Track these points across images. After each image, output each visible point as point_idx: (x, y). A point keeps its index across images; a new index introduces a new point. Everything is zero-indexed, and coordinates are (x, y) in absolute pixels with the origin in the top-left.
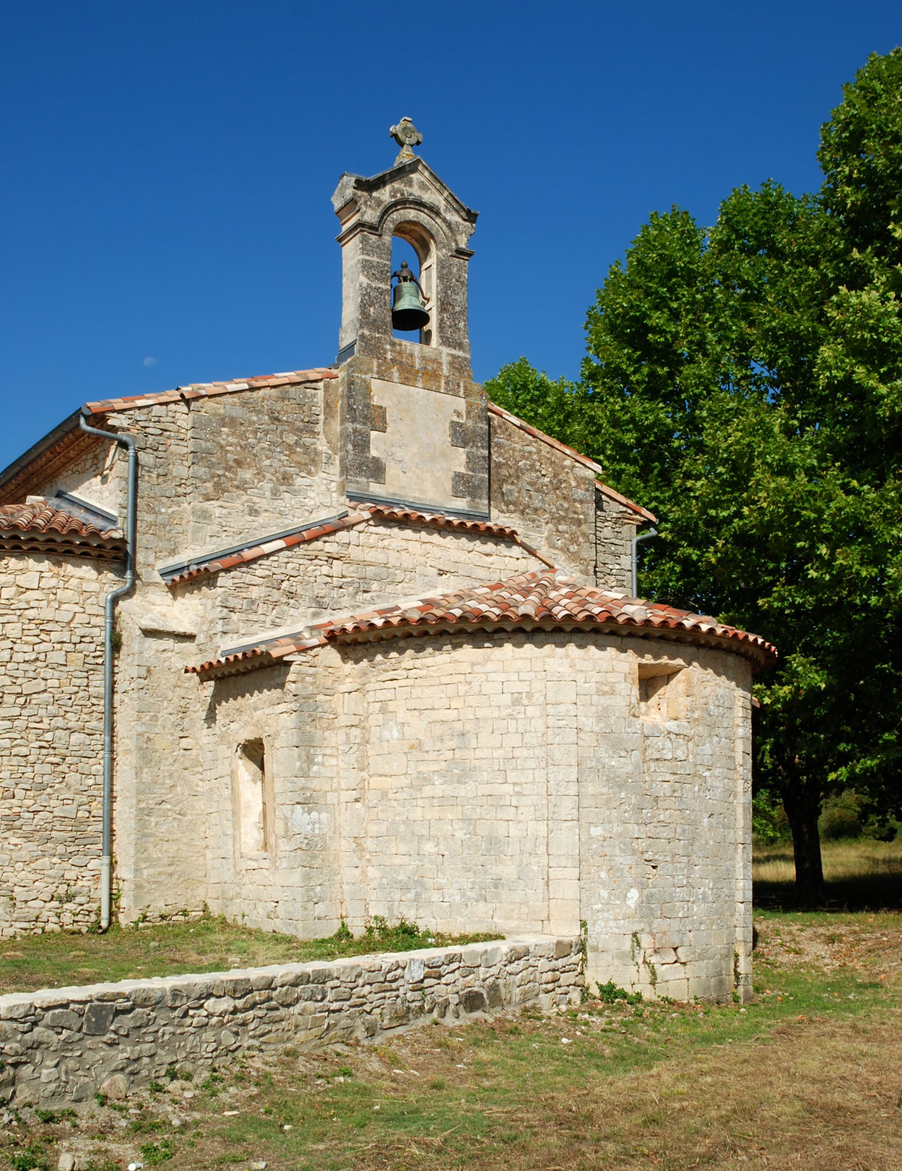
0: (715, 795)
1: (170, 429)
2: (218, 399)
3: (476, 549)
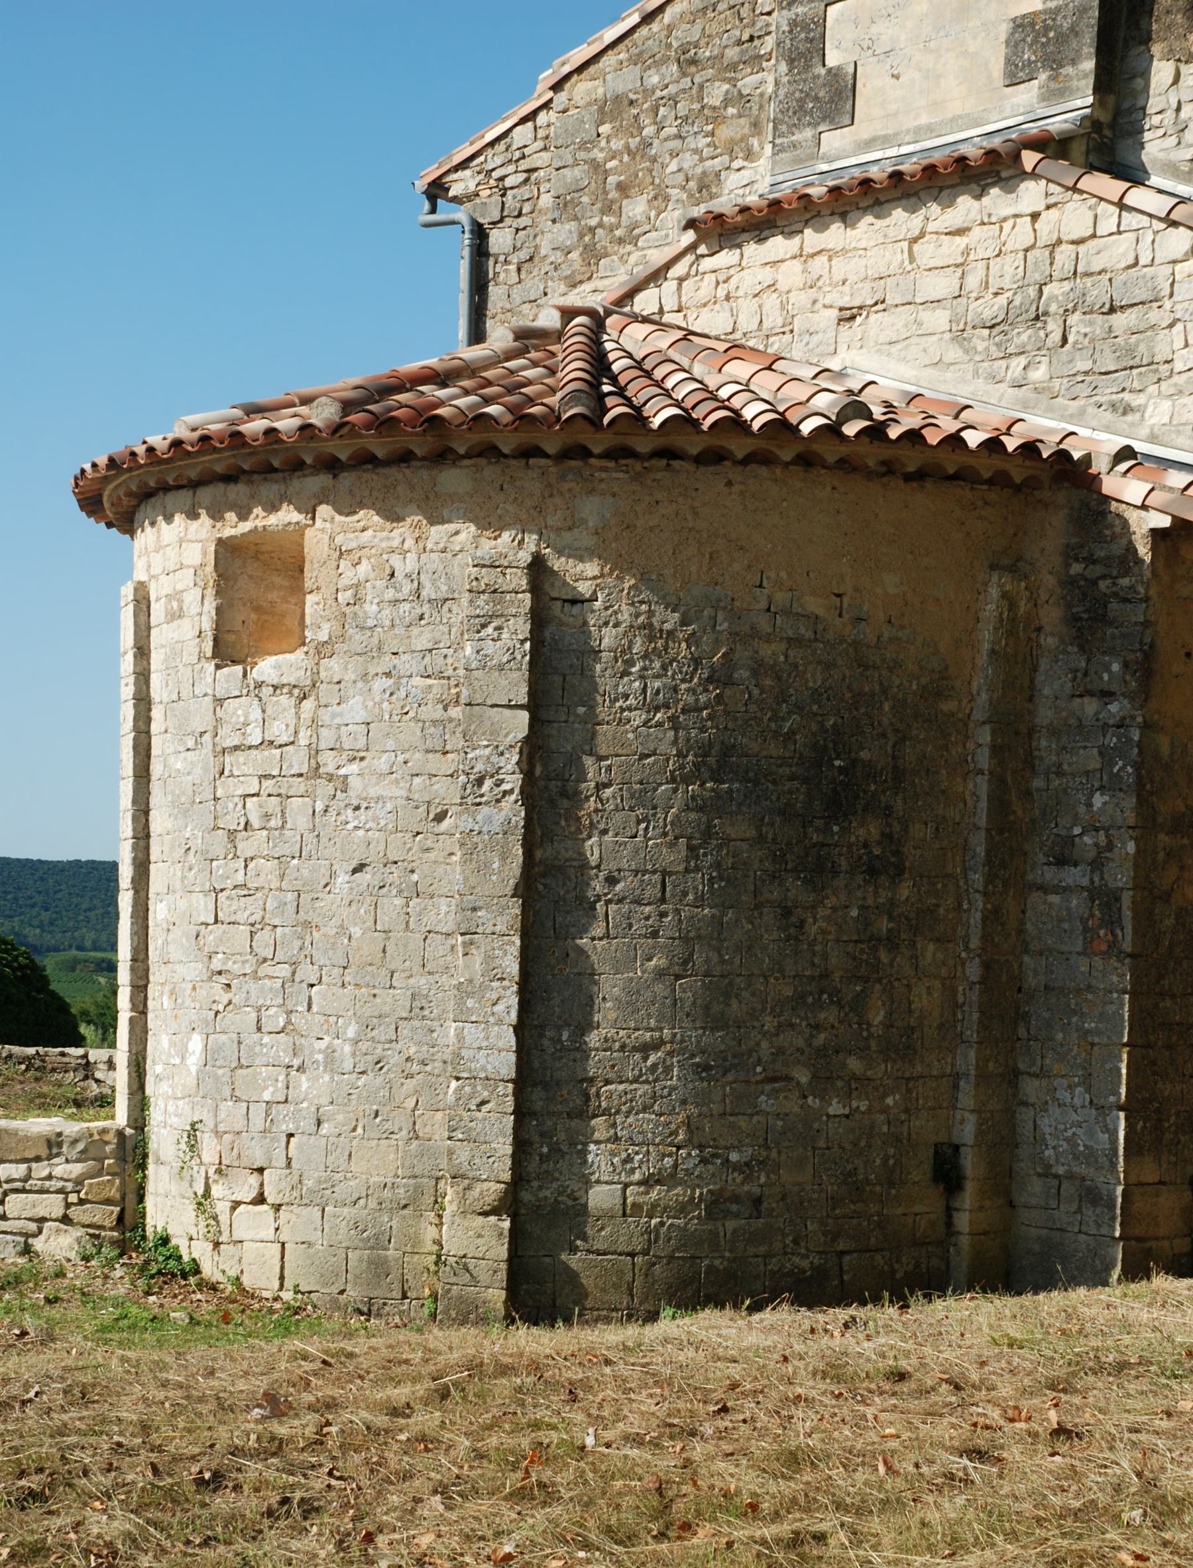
0: (375, 819)
1: (538, 165)
2: (592, 69)
3: (931, 227)
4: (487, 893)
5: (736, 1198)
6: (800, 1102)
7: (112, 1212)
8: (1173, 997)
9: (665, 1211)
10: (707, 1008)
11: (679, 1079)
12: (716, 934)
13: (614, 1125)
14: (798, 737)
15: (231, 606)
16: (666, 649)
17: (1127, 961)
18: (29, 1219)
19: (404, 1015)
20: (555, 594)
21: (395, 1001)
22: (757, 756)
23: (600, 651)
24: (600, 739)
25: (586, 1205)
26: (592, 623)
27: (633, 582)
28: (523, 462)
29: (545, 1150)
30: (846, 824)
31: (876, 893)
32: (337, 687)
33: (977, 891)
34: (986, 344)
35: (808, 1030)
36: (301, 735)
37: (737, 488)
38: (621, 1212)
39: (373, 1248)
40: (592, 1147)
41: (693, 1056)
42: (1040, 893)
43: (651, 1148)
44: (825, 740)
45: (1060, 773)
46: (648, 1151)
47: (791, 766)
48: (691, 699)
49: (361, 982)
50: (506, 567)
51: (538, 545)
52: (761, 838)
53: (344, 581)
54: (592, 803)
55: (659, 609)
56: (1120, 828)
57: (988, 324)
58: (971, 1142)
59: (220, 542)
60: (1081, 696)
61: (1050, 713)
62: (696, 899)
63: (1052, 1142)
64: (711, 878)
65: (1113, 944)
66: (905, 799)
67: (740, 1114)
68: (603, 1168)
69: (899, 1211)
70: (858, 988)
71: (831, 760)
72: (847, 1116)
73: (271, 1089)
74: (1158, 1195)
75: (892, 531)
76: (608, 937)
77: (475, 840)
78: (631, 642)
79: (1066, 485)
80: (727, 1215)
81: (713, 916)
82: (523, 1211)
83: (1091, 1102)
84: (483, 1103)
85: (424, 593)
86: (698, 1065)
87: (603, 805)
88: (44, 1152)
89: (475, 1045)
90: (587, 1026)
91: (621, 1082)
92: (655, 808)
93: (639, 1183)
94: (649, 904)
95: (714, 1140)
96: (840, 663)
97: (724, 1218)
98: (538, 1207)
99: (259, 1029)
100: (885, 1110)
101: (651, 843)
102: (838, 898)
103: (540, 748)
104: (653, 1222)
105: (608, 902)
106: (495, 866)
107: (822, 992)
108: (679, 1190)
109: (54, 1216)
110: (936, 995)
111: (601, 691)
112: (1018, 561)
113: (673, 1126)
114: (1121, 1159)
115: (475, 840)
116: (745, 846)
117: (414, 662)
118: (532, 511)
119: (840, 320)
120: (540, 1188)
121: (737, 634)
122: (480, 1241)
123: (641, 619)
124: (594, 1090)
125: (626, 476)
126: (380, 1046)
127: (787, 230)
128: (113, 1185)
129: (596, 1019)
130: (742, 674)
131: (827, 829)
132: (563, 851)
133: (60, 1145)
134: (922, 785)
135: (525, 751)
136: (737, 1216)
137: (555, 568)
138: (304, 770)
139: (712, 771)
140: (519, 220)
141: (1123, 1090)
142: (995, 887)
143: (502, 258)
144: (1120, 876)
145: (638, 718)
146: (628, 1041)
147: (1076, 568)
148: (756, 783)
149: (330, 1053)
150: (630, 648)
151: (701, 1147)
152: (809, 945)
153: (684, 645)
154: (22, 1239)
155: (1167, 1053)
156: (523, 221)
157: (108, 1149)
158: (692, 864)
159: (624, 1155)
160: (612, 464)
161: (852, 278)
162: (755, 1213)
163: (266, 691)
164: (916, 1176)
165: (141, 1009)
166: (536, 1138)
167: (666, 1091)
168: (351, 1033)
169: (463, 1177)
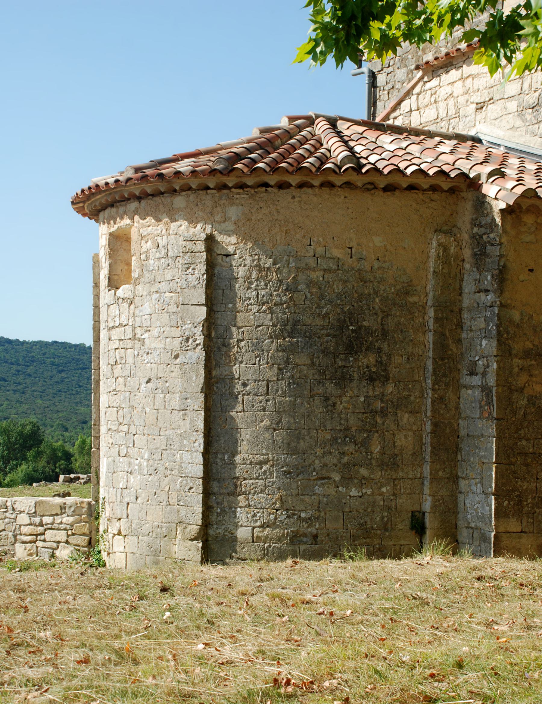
4: (191, 391)
5: (305, 535)
6: (335, 489)
7: (85, 540)
8: (528, 440)
9: (271, 539)
10: (289, 444)
11: (276, 478)
12: (292, 410)
13: (248, 499)
14: (330, 316)
15: (116, 263)
16: (267, 276)
17: (495, 421)
18: (54, 542)
19: (164, 448)
20: (219, 252)
21: (160, 442)
22: (310, 325)
23: (238, 278)
24: (238, 319)
25: (236, 537)
26: (234, 265)
27: (251, 245)
28: (205, 191)
29: (219, 510)
30: (356, 357)
31: (374, 389)
32: (141, 298)
33: (430, 388)
34: (530, 116)
35: (339, 455)
36: (130, 320)
37: (297, 199)
38: (251, 540)
39: (154, 556)
40: (239, 509)
41: (283, 467)
42: (465, 389)
43: (265, 510)
44: (345, 317)
45: (471, 330)
46: (263, 512)
47: (327, 329)
48: (278, 299)
49: (149, 433)
50: (196, 241)
51: (212, 230)
52: (313, 364)
53: (143, 250)
54: (236, 349)
55: (263, 258)
56: (491, 356)
57: (531, 107)
58: (428, 510)
59: (111, 234)
60: (479, 292)
61: (468, 301)
62: (282, 393)
63: (470, 512)
64: (289, 383)
65: (490, 414)
66: (389, 344)
67: (305, 495)
68: (243, 519)
69: (391, 543)
70: (365, 435)
71: (348, 326)
72: (360, 497)
73: (122, 482)
74: (520, 538)
75: (377, 216)
76: (244, 411)
77: (186, 367)
78: (251, 273)
79: (472, 189)
80: (301, 542)
81: (291, 401)
82: (210, 539)
83: (483, 491)
84: (191, 488)
85: (169, 254)
86: (285, 471)
87: (240, 349)
88: (59, 512)
89: (187, 462)
90: (234, 453)
91: (251, 479)
92: (263, 350)
93: (260, 527)
94: (261, 395)
95: (294, 507)
96: (351, 280)
97: (299, 544)
98: (217, 537)
99: (119, 455)
100: (382, 494)
101: (261, 367)
102: (353, 392)
103: (214, 324)
104: (266, 545)
105: (243, 395)
106: (194, 379)
107: (346, 437)
108: (277, 530)
109: (63, 540)
110: (410, 439)
111: (239, 297)
112: (454, 227)
113: (274, 500)
114: (493, 519)
115: (186, 367)
116: (305, 368)
117: (166, 286)
118: (208, 214)
119: (477, 109)
120: (217, 528)
121: (299, 268)
122: (190, 553)
123: (255, 262)
124: (239, 483)
125: (247, 196)
126: (156, 462)
127: (457, 66)
128: (86, 527)
129: (239, 450)
130: (302, 287)
131: (346, 359)
132: (224, 371)
133: (65, 508)
134: (399, 338)
135: (205, 326)
136: (305, 543)
137: (219, 240)
138: (131, 337)
139: (289, 332)
140: (389, 69)
141: (493, 485)
142: (439, 386)
143: (382, 88)
144: (492, 381)
145: (255, 308)
146: (253, 460)
147: (475, 230)
148: (310, 338)
149: (140, 465)
150: (250, 276)
151: (287, 510)
152: (338, 414)
153: (274, 274)
154: (51, 551)
155: (525, 468)
156: (390, 69)
157: (84, 510)
158: (280, 376)
159: (252, 513)
160: (241, 191)
161: (481, 88)
162: (314, 542)
163: (121, 300)
164: (400, 526)
165: (98, 447)
166: (215, 505)
167: (270, 484)
168: (146, 457)
169: (183, 523)
